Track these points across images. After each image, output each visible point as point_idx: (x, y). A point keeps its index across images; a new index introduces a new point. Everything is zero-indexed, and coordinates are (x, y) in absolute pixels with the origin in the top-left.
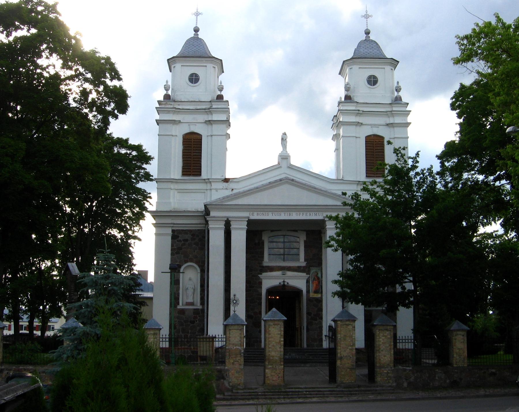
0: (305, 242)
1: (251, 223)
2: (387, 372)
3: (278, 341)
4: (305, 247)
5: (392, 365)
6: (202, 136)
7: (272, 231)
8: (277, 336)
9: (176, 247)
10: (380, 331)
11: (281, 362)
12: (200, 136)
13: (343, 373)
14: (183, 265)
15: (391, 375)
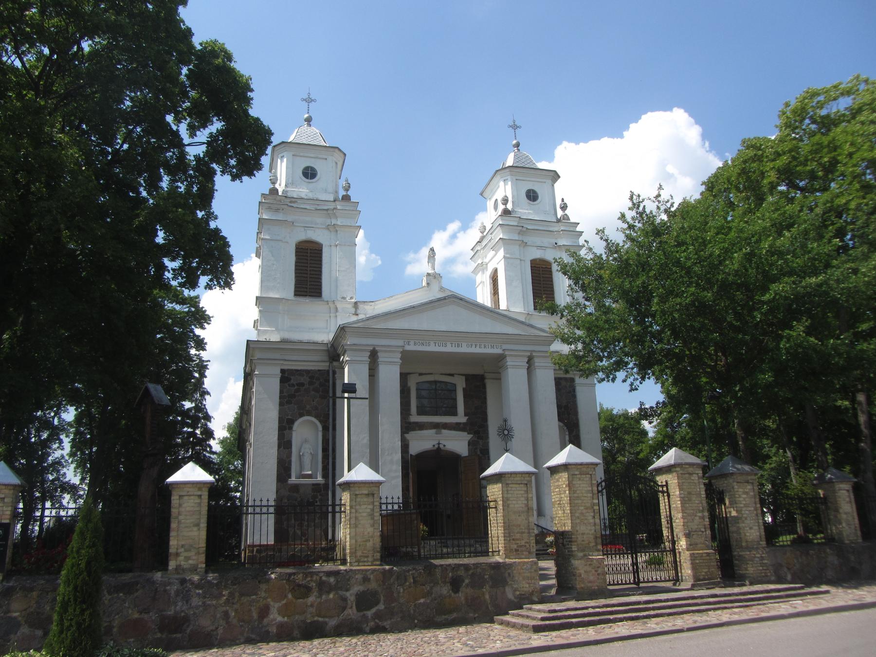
1: (407, 357)
3: (589, 505)
4: (465, 397)
5: (764, 543)
6: (322, 245)
7: (421, 374)
9: (286, 394)
11: (597, 544)
13: (698, 561)
14: (296, 420)
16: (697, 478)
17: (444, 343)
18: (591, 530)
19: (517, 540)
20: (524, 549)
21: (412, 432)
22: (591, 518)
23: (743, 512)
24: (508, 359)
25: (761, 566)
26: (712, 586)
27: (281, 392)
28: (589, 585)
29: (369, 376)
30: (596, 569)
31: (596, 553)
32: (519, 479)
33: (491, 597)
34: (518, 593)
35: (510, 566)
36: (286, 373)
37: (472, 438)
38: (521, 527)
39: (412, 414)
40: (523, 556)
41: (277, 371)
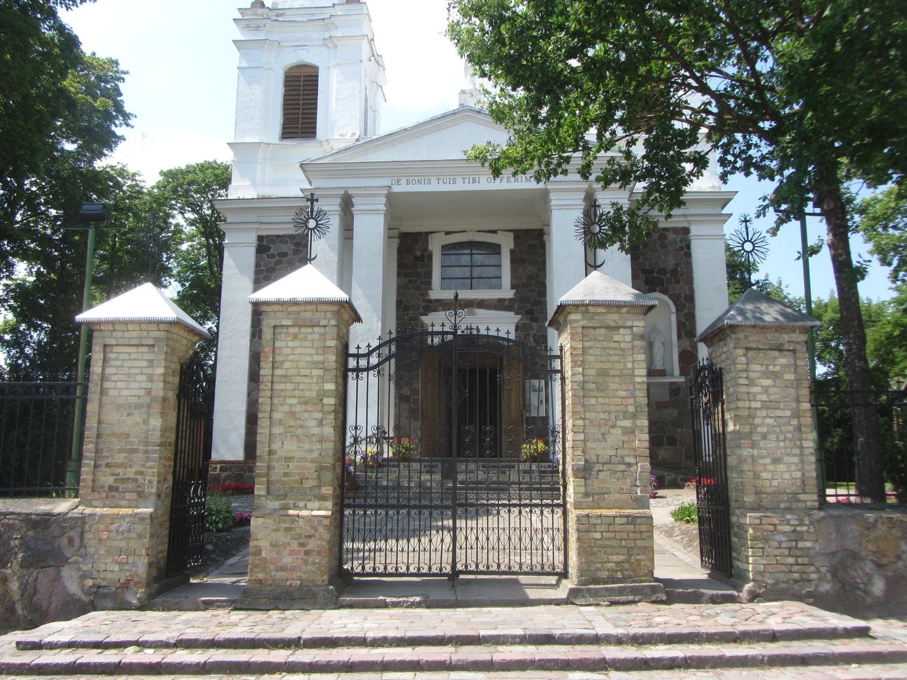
0: (512, 252)
2: (794, 531)
7: (448, 233)
8: (307, 372)
9: (263, 268)
10: (751, 354)
12: (315, 69)
13: (598, 536)
15: (808, 544)
16: (628, 338)
17: (452, 178)
18: (310, 451)
19: (117, 466)
20: (130, 486)
21: (433, 313)
22: (313, 423)
23: (757, 421)
24: (552, 196)
25: (790, 555)
26: (631, 598)
27: (257, 265)
28: (281, 575)
29: (352, 238)
30: (303, 540)
31: (316, 504)
32: (135, 334)
33: (23, 588)
34: (90, 582)
35: (82, 520)
36: (265, 240)
37: (521, 319)
38: (131, 439)
39: (433, 288)
40: (125, 503)
41: (252, 239)
